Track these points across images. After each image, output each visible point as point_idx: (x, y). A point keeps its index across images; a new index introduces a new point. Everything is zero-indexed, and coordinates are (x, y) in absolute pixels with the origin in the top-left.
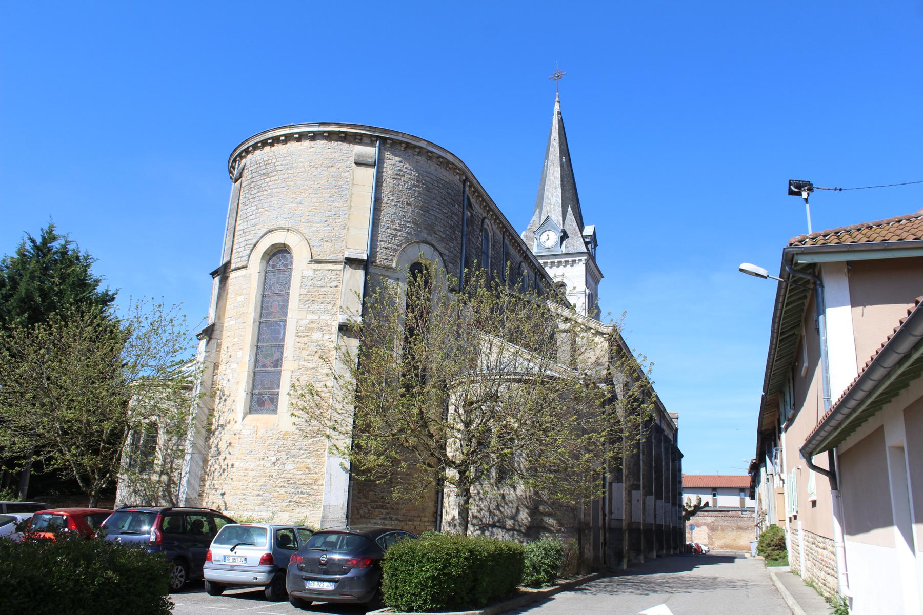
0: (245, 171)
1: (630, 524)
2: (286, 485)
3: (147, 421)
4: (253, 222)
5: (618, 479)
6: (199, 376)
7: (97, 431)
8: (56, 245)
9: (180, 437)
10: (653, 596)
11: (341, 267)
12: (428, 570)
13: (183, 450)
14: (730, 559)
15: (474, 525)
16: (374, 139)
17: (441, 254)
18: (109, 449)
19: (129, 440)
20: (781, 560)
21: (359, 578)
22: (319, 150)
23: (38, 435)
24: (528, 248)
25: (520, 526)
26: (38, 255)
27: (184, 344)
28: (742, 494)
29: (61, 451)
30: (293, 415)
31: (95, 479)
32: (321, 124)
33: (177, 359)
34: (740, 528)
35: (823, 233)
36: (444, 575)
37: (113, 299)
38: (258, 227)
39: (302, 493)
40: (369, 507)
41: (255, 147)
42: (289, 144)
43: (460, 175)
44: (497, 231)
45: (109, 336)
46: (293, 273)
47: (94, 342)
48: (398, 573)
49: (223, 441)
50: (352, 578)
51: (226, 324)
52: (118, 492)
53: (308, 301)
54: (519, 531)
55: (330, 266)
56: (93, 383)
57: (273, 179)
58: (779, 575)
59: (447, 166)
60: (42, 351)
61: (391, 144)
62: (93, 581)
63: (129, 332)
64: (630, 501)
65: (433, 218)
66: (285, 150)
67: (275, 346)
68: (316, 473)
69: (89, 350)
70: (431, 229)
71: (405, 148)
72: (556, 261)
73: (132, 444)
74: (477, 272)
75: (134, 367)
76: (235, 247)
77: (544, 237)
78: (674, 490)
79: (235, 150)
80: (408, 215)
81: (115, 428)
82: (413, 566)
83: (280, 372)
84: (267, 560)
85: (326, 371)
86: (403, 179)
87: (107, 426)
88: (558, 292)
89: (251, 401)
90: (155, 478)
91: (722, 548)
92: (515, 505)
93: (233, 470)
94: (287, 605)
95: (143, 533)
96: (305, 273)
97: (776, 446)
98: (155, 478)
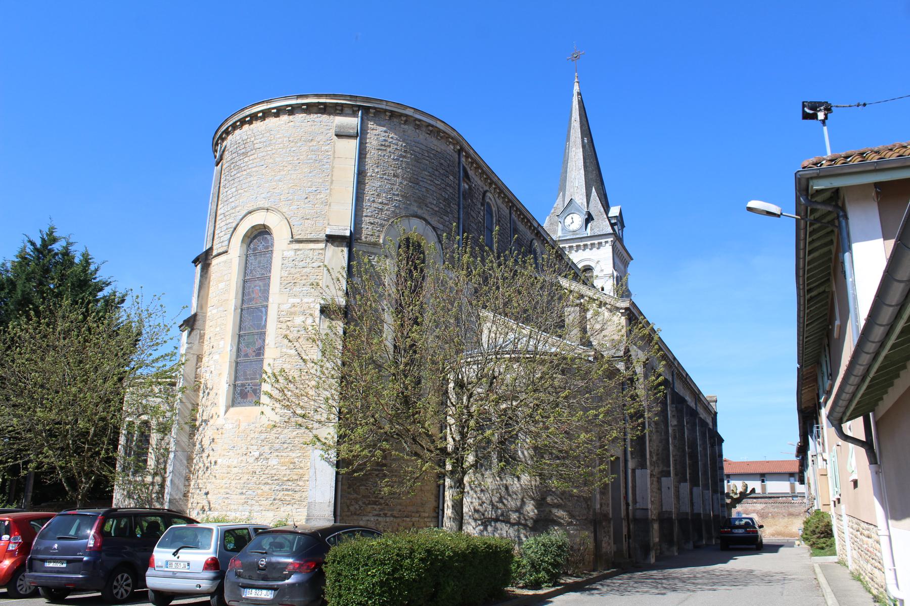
0: (226, 153)
2: (270, 482)
5: (643, 465)
8: (57, 247)
11: (322, 245)
12: (376, 574)
15: (475, 520)
16: (355, 109)
17: (434, 228)
22: (298, 124)
24: (539, 225)
25: (526, 520)
26: (39, 258)
28: (792, 479)
32: (299, 97)
34: (791, 515)
35: (843, 154)
36: (395, 579)
38: (238, 209)
39: (287, 490)
40: (360, 503)
41: (234, 127)
42: (267, 120)
43: (454, 144)
44: (503, 206)
46: (274, 255)
48: (341, 578)
49: (207, 437)
51: (209, 314)
53: (289, 284)
55: (312, 246)
57: (251, 158)
58: (823, 567)
59: (438, 135)
61: (374, 113)
64: (660, 489)
65: (424, 190)
68: (301, 468)
70: (421, 202)
71: (391, 117)
72: (582, 244)
76: (217, 232)
77: (568, 220)
78: (714, 476)
80: (396, 187)
82: (358, 569)
84: (212, 565)
86: (388, 150)
88: (584, 275)
89: (234, 394)
91: (773, 535)
92: (520, 496)
96: (286, 254)
97: (817, 423)
98: (149, 479)
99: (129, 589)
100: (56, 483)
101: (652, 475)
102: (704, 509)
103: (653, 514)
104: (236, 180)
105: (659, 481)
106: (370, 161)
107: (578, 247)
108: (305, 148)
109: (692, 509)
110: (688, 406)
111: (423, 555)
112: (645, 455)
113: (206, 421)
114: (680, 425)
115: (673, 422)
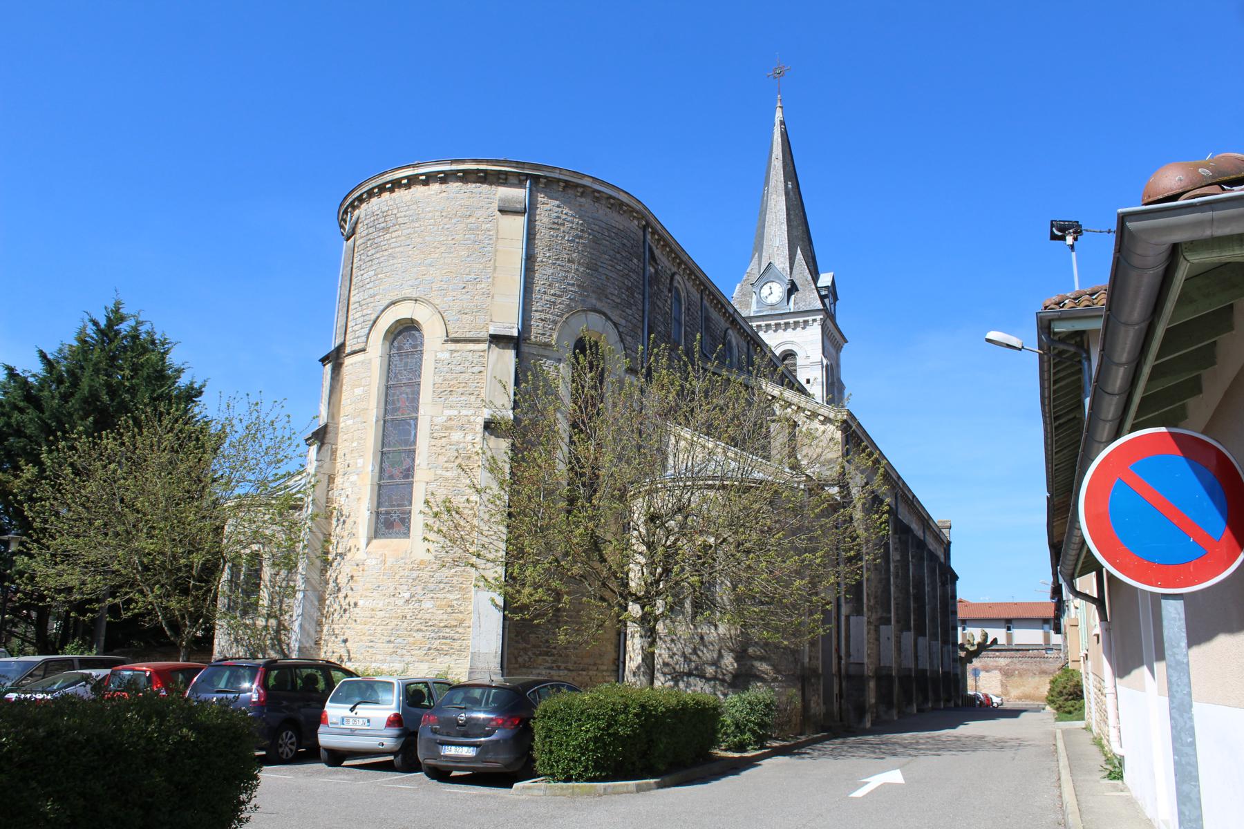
0: (360, 225)
1: (878, 669)
3: (248, 551)
4: (371, 291)
5: (858, 611)
6: (310, 492)
7: (186, 566)
8: (124, 327)
9: (290, 570)
10: (890, 760)
11: (484, 346)
12: (589, 730)
13: (293, 588)
14: (1014, 713)
15: (664, 674)
17: (615, 324)
18: (201, 588)
19: (226, 575)
20: (1076, 713)
21: (505, 741)
22: (452, 195)
23: (113, 572)
26: (103, 342)
27: (290, 452)
28: (1046, 626)
29: (141, 592)
30: (425, 539)
31: (186, 625)
33: (281, 472)
35: (1089, 290)
36: (610, 735)
37: (200, 393)
42: (413, 189)
43: (638, 219)
44: (693, 291)
45: (196, 442)
46: (425, 357)
47: (177, 452)
48: (552, 734)
50: (497, 742)
51: (342, 425)
52: (216, 641)
53: (444, 392)
54: (723, 681)
55: (471, 346)
56: (178, 504)
57: (394, 235)
60: (112, 466)
61: (545, 184)
62: (167, 741)
63: (220, 438)
64: (878, 639)
65: (604, 277)
66: (409, 197)
67: (405, 451)
69: (171, 463)
70: (601, 293)
71: (564, 188)
72: (782, 322)
73: (231, 581)
74: (655, 350)
75: (230, 481)
76: (350, 324)
79: (345, 198)
81: (208, 560)
82: (570, 725)
83: (412, 484)
84: (395, 721)
85: (468, 481)
87: (198, 560)
88: (783, 369)
90: (261, 622)
91: (1020, 699)
93: (356, 610)
94: (421, 776)
95: (244, 691)
96: (439, 355)
98: (261, 622)
99: (294, 748)
100: (155, 627)
101: (869, 623)
102: (931, 664)
103: (869, 670)
104: (375, 262)
105: (877, 630)
106: (539, 243)
107: (778, 325)
108: (461, 226)
109: (916, 664)
110: (915, 536)
111: (637, 710)
112: (861, 599)
113: (342, 555)
114: (904, 563)
115: (895, 556)
